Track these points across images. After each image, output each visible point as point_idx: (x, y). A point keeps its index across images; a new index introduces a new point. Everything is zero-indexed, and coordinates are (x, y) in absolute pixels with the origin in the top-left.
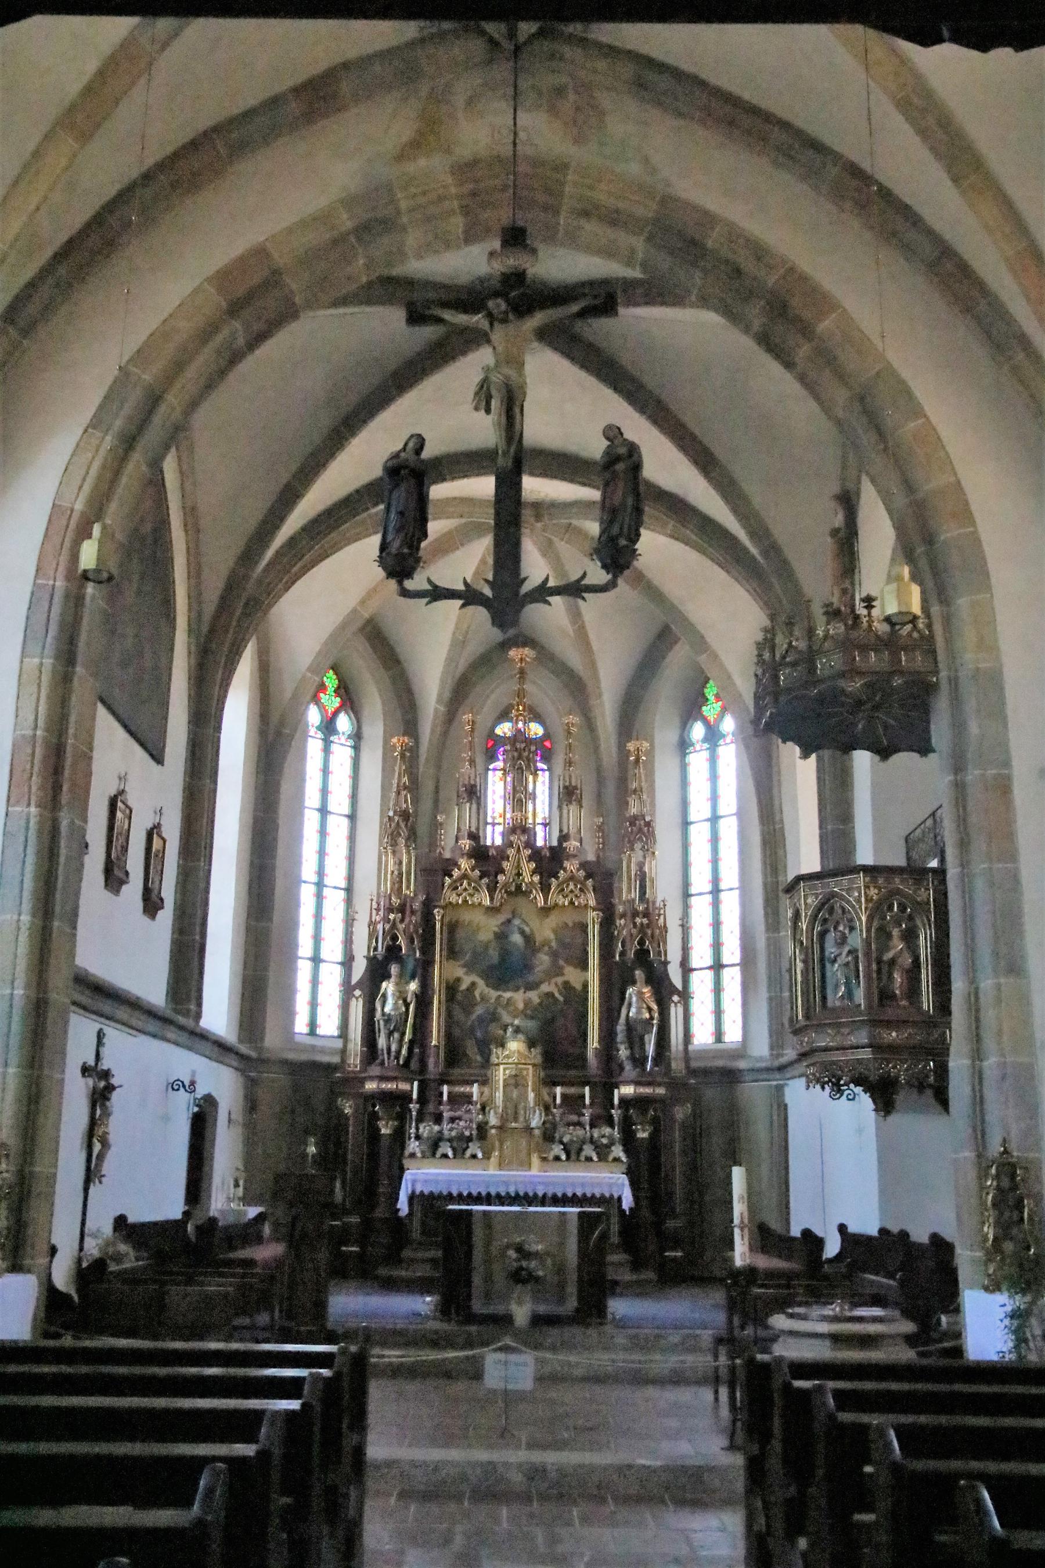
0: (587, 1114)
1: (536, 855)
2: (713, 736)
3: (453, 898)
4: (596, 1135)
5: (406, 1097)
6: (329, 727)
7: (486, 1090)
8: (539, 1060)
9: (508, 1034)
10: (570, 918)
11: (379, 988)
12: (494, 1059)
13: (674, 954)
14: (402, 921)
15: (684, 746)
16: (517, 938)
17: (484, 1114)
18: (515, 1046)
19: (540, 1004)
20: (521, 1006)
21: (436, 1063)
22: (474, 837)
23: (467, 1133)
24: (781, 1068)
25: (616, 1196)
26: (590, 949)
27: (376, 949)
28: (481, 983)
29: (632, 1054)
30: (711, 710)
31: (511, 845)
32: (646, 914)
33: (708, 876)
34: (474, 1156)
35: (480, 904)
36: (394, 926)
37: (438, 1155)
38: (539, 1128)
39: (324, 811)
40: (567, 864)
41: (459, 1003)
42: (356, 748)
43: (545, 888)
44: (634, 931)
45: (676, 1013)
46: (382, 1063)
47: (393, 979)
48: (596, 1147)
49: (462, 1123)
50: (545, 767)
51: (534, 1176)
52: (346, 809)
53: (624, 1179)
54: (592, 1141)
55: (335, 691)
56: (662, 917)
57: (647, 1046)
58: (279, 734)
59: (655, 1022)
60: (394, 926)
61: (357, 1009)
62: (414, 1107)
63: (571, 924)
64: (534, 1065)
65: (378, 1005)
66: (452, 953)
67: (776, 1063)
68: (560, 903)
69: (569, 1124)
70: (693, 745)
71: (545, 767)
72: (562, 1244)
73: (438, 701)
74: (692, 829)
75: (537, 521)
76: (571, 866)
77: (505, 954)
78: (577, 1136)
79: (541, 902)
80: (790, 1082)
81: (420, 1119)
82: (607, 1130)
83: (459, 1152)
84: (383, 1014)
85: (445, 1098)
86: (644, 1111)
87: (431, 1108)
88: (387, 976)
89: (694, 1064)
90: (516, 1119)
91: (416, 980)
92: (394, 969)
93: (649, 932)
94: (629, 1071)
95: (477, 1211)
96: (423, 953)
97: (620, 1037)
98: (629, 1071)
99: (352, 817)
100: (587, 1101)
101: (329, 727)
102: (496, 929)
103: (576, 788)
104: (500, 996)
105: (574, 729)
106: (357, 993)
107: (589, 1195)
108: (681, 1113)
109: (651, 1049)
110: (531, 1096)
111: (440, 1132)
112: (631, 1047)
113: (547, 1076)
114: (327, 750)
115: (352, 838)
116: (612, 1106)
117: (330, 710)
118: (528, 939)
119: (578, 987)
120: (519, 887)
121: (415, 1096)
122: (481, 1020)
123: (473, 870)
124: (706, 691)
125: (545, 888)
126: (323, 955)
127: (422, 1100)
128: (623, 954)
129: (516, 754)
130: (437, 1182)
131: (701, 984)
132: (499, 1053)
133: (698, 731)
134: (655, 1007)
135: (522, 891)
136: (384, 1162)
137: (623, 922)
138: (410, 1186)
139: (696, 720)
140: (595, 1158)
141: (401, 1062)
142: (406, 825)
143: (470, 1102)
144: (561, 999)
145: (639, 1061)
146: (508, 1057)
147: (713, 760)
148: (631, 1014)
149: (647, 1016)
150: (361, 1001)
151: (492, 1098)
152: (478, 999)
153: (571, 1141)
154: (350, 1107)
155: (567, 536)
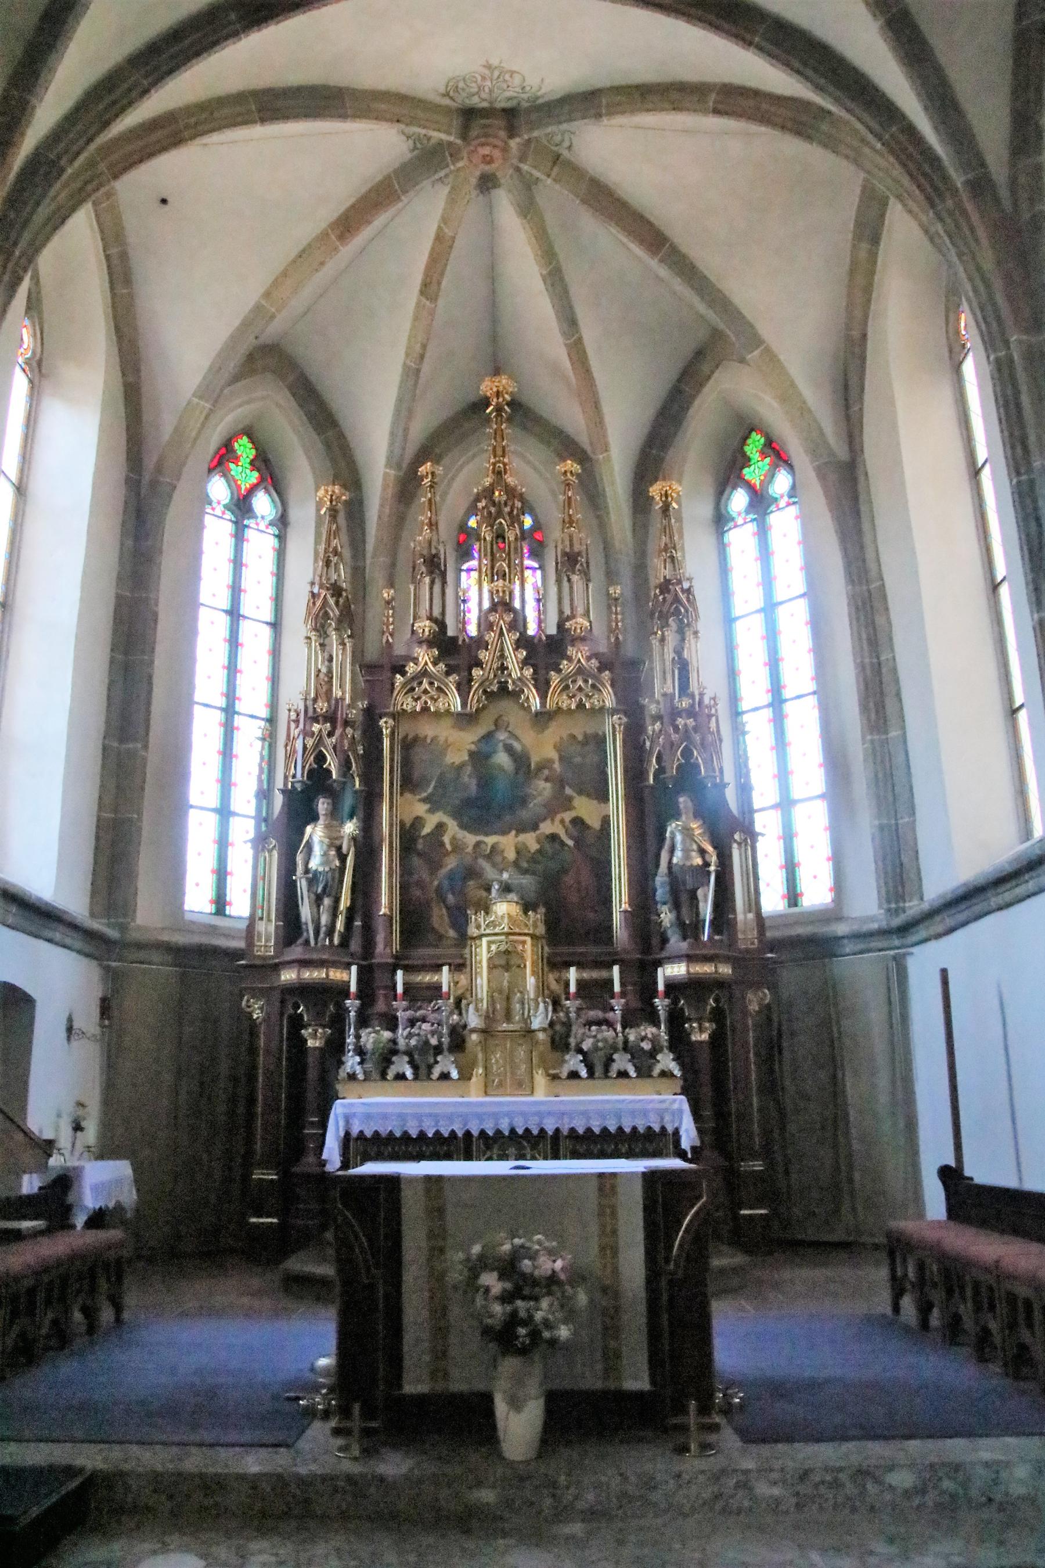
0: (618, 1004)
1: (524, 642)
3: (408, 704)
4: (632, 1038)
5: (343, 991)
6: (241, 506)
7: (463, 979)
8: (541, 930)
9: (494, 892)
10: (580, 728)
11: (303, 834)
12: (472, 931)
14: (330, 734)
15: (721, 521)
16: (502, 759)
17: (460, 1014)
18: (504, 909)
19: (539, 851)
20: (511, 855)
21: (388, 943)
23: (434, 1041)
24: (904, 930)
25: (670, 1129)
26: (610, 771)
28: (452, 827)
29: (678, 917)
30: (754, 473)
31: (490, 627)
32: (691, 713)
33: (765, 683)
34: (445, 1076)
36: (320, 742)
37: (390, 1075)
38: (544, 1030)
39: (234, 614)
40: (571, 651)
42: (281, 538)
43: (543, 687)
44: (675, 737)
46: (307, 942)
47: (322, 821)
48: (633, 1057)
49: (426, 1026)
50: (536, 565)
51: (542, 1103)
53: (682, 1103)
54: (626, 1047)
55: (252, 463)
56: (714, 719)
57: (701, 905)
58: (154, 484)
59: (712, 868)
60: (320, 742)
62: (352, 1004)
63: (580, 738)
64: (533, 937)
65: (300, 859)
66: (409, 783)
67: (897, 921)
68: (564, 706)
69: (589, 1024)
70: (733, 519)
71: (536, 565)
72: (610, 1249)
73: (388, 465)
74: (739, 627)
75: (511, 136)
76: (578, 653)
77: (486, 781)
78: (605, 1040)
79: (535, 703)
80: (914, 950)
81: (363, 1021)
82: (650, 1031)
83: (422, 1071)
84: (307, 871)
85: (400, 989)
86: (702, 1000)
87: (380, 1006)
89: (769, 934)
90: (508, 1017)
91: (355, 820)
92: (322, 805)
93: (697, 738)
94: (676, 943)
95: (413, 1180)
96: (365, 779)
97: (661, 892)
98: (676, 943)
99: (276, 625)
100: (617, 988)
101: (241, 506)
102: (473, 747)
103: (579, 554)
107: (641, 1130)
108: (754, 1001)
109: (707, 910)
110: (531, 981)
111: (394, 1041)
112: (677, 906)
114: (239, 536)
115: (276, 653)
116: (654, 993)
117: (244, 486)
118: (520, 760)
119: (595, 824)
120: (503, 687)
121: (353, 988)
122: (451, 876)
124: (747, 449)
126: (234, 806)
127: (366, 994)
128: (660, 771)
129: (493, 510)
130: (385, 1117)
132: (481, 920)
133: (739, 500)
134: (709, 848)
135: (509, 693)
136: (309, 1087)
137: (657, 726)
138: (342, 1123)
139: (734, 488)
140: (633, 1073)
141: (336, 941)
142: (337, 603)
143: (440, 997)
144: (570, 843)
145: (690, 929)
146: (493, 925)
147: (763, 532)
148: (675, 860)
149: (698, 861)
150: (275, 853)
151: (470, 988)
152: (449, 847)
153: (596, 1049)
154: (261, 1008)
155: (556, 170)
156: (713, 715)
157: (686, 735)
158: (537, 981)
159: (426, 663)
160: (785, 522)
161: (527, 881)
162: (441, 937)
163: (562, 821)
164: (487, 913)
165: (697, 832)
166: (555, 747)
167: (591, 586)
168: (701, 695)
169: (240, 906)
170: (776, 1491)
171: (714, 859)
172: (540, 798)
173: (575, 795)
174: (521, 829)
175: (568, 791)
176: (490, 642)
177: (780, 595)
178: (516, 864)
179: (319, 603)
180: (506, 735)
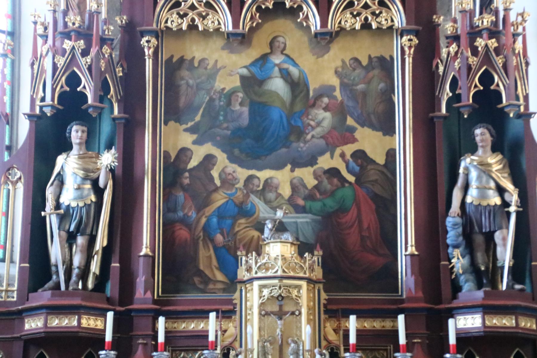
8: (318, 273)
16: (278, 85)
20: (286, 191)
28: (221, 157)
32: (493, 33)
35: (217, 30)
41: (184, 189)
77: (259, 108)
84: (58, 206)
92: (76, 133)
113: (329, 301)
118: (297, 86)
122: (221, 213)
134: (508, 185)
144: (351, 179)
156: (518, 35)
157: (487, 59)
161: (303, 219)
162: (206, 280)
163: (343, 155)
165: (496, 168)
166: (336, 72)
171: (513, 197)
172: (319, 130)
174: (296, 164)
175: (350, 121)
178: (291, 201)
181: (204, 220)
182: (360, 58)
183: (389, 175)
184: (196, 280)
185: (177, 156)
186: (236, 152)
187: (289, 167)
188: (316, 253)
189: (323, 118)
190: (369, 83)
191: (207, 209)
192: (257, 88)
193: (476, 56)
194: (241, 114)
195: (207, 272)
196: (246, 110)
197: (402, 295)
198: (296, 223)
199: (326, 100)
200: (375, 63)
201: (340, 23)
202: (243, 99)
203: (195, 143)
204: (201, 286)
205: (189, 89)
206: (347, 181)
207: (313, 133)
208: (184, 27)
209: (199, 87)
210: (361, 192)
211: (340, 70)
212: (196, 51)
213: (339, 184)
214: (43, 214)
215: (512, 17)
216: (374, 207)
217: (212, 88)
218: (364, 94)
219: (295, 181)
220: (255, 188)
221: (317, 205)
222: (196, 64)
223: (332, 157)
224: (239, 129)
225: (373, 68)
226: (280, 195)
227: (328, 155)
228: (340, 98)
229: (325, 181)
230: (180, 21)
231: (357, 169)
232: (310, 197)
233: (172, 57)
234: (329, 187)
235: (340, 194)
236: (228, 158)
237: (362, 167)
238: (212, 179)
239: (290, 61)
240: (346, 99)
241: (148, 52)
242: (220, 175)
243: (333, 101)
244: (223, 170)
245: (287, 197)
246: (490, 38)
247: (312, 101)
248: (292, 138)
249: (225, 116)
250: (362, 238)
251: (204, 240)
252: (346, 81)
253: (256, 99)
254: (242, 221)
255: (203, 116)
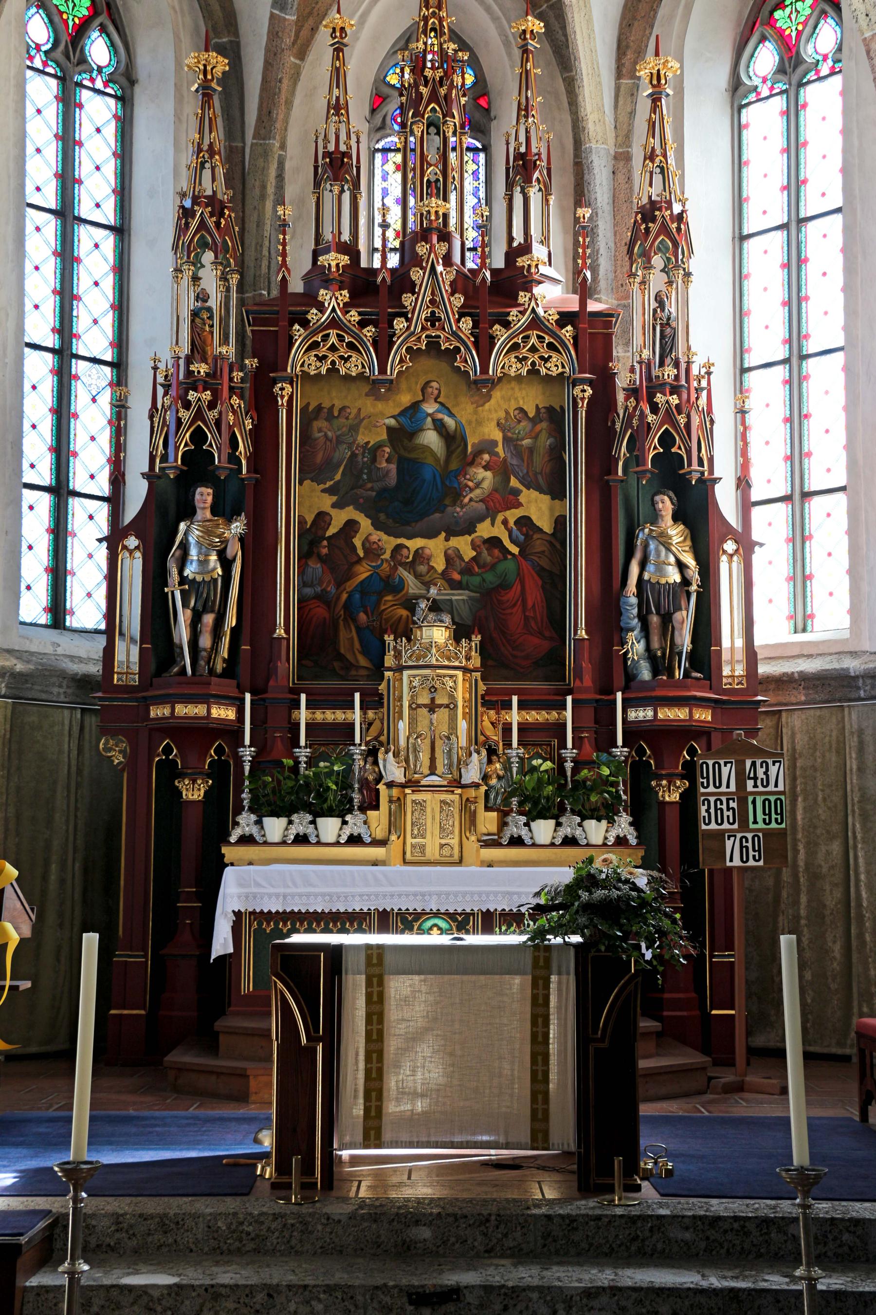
2: (793, 69)
8: (476, 661)
13: (724, 468)
16: (430, 438)
20: (440, 564)
22: (350, 249)
27: (164, 458)
28: (365, 523)
33: (780, 331)
35: (361, 376)
42: (125, 100)
45: (728, 572)
52: (108, 214)
59: (694, 587)
61: (133, 568)
77: (410, 463)
84: (183, 580)
88: (188, 512)
89: (763, 669)
92: (204, 496)
93: (682, 420)
104: (399, 547)
105: (533, 44)
106: (132, 542)
109: (685, 640)
113: (488, 692)
118: (453, 439)
123: (346, 310)
125: (484, 344)
131: (770, 526)
133: (765, 59)
134: (689, 560)
139: (763, 39)
144: (515, 550)
147: (793, 113)
156: (703, 389)
157: (669, 417)
158: (469, 724)
159: (334, 310)
160: (824, 99)
161: (459, 596)
162: (349, 666)
163: (505, 522)
164: (409, 640)
165: (676, 540)
166: (498, 424)
167: (552, 200)
168: (689, 363)
169: (87, 611)
170: (688, 1236)
172: (478, 492)
173: (521, 487)
174: (452, 532)
175: (514, 482)
176: (418, 282)
177: (811, 205)
179: (194, 224)
180: (436, 406)
181: (345, 596)
182: (525, 408)
183: (558, 546)
184: (337, 665)
185: (314, 522)
186: (382, 517)
187: (443, 534)
188: (473, 637)
189: (484, 478)
190: (536, 438)
191: (348, 584)
192: (406, 441)
193: (656, 414)
194: (388, 472)
195: (349, 656)
196: (393, 467)
197: (569, 684)
198: (451, 600)
199: (486, 457)
200: (543, 414)
201: (503, 367)
202: (389, 454)
203: (334, 506)
204: (342, 673)
205: (328, 443)
206: (510, 553)
207: (472, 495)
208: (324, 371)
209: (339, 441)
210: (526, 565)
211: (503, 421)
212: (333, 397)
213: (501, 555)
214: (166, 590)
215: (695, 370)
216: (540, 583)
217: (354, 442)
218: (531, 450)
219: (450, 552)
220: (404, 560)
221: (476, 580)
222: (336, 414)
223: (493, 525)
224: (385, 490)
225: (541, 421)
226: (433, 567)
227: (488, 521)
228: (502, 455)
229: (485, 552)
230: (319, 364)
231: (522, 538)
232: (467, 570)
233: (308, 404)
234: (489, 559)
235: (501, 567)
236: (372, 524)
237: (526, 535)
238: (354, 548)
239: (445, 411)
240: (509, 455)
241: (282, 402)
242: (363, 545)
243: (494, 458)
244: (367, 539)
245: (440, 571)
246: (671, 394)
247: (470, 458)
248: (447, 502)
249: (369, 474)
250: (526, 618)
251: (345, 620)
252: (509, 434)
253: (402, 452)
254: (389, 598)
255: (343, 474)
